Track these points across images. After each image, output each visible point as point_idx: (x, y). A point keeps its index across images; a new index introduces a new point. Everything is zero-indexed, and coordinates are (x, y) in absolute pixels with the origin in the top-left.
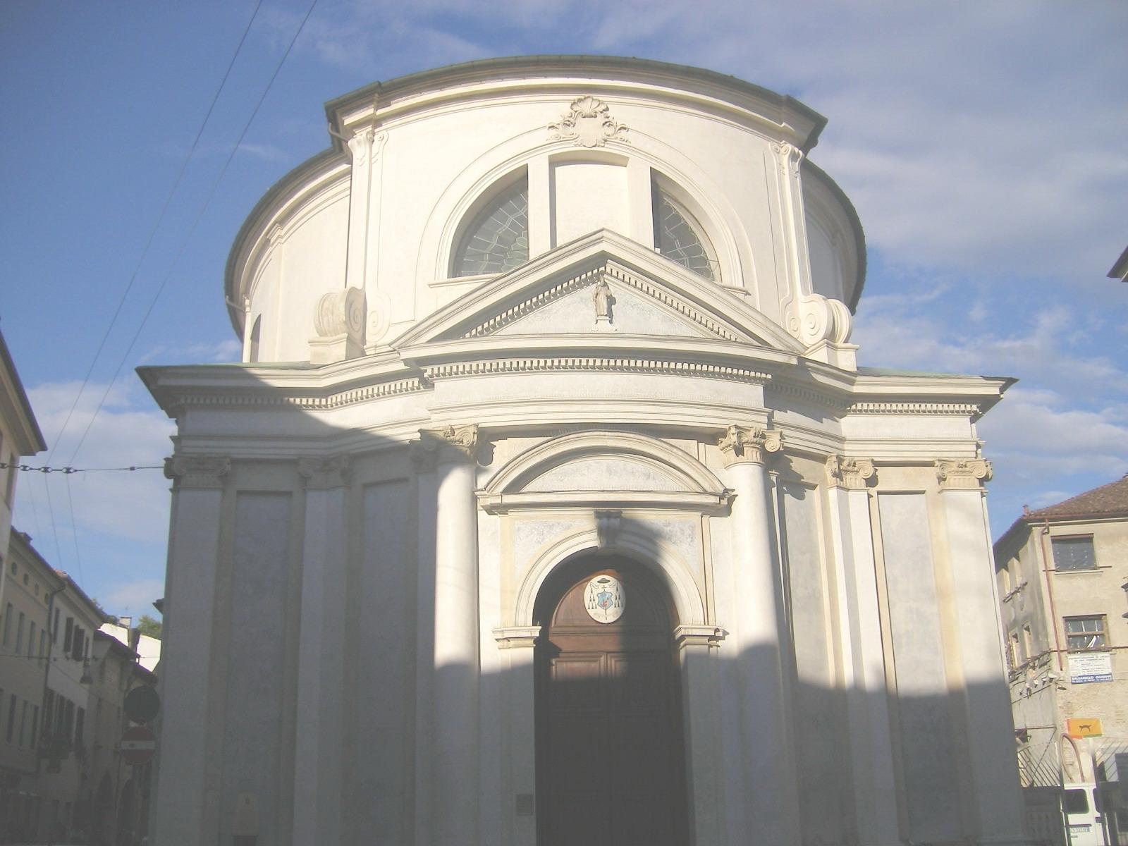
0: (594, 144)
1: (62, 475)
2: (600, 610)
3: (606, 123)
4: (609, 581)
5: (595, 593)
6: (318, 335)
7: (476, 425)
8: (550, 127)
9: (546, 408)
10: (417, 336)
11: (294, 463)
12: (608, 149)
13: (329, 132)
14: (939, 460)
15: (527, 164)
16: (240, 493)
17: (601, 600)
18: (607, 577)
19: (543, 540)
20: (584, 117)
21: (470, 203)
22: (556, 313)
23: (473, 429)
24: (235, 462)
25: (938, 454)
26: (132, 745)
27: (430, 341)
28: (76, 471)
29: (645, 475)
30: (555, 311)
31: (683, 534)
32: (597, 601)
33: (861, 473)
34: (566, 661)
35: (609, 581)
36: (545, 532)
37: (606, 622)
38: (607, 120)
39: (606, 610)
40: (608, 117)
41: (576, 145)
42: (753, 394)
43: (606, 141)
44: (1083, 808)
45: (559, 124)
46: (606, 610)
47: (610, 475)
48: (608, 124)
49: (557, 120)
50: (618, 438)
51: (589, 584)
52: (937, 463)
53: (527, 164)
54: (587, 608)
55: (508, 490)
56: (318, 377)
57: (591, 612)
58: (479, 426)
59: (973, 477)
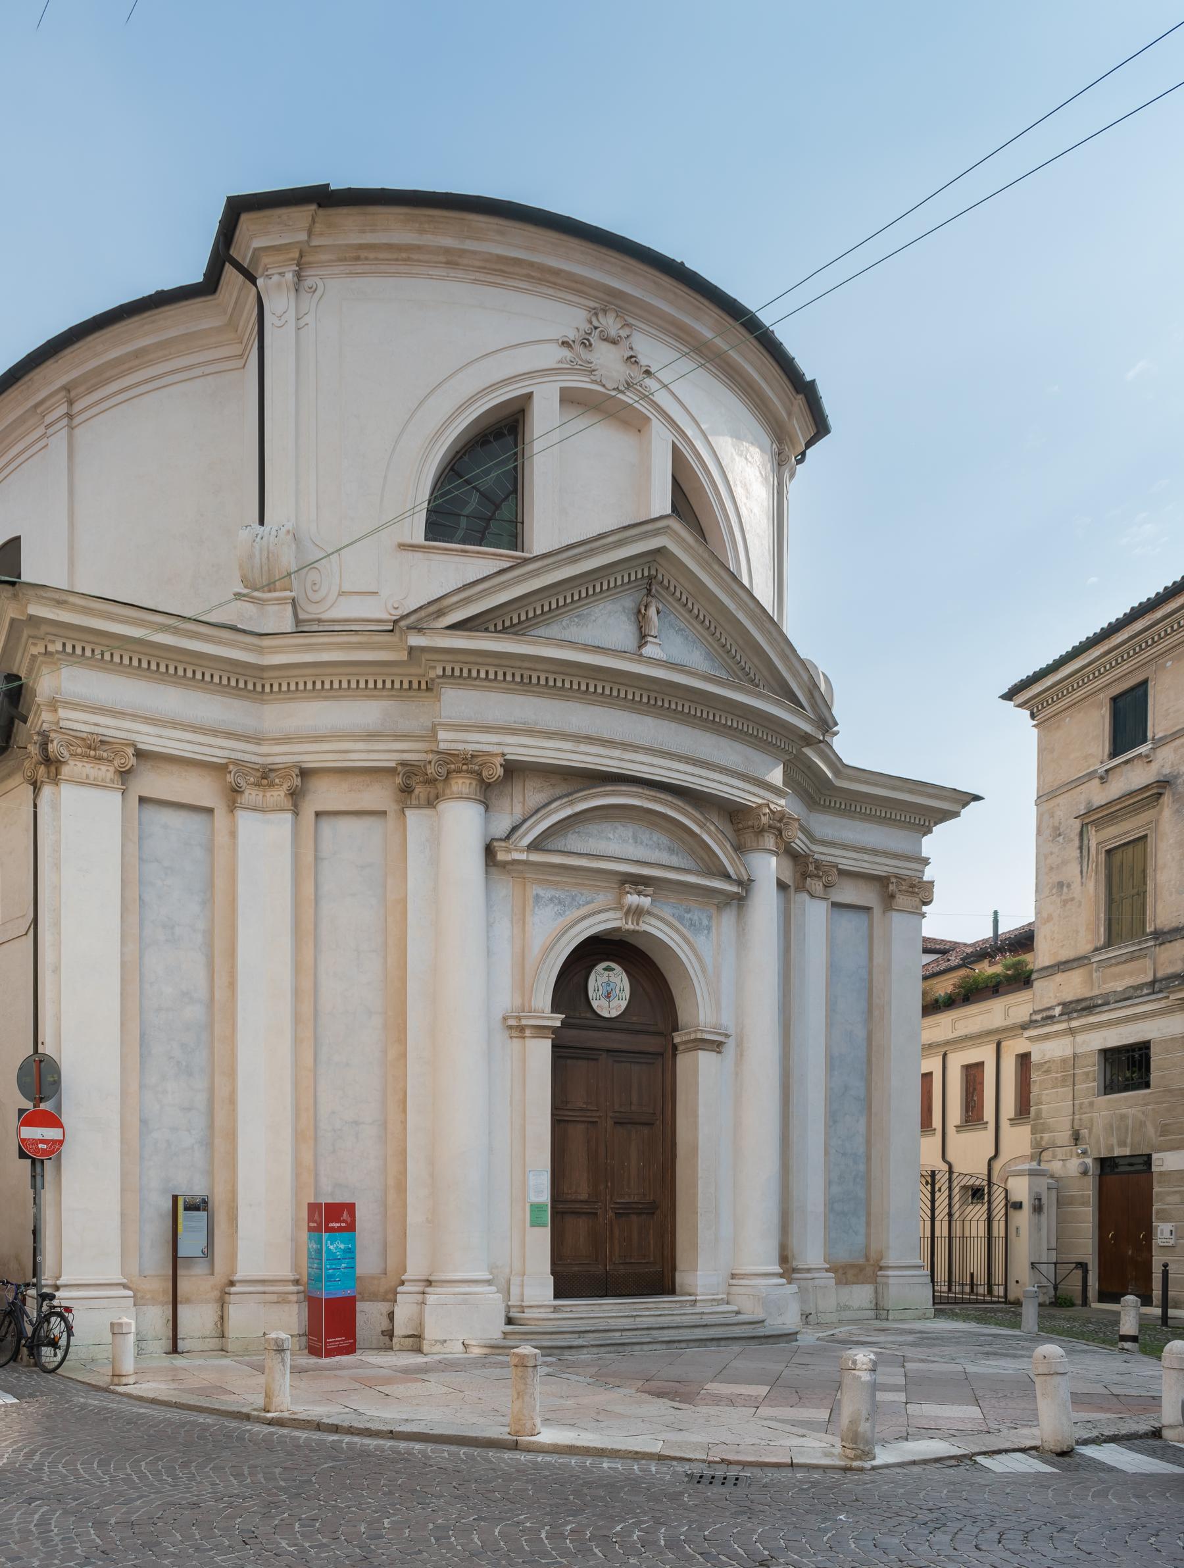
2: (604, 1002)
5: (599, 982)
7: (504, 755)
8: (563, 343)
9: (583, 748)
10: (440, 613)
11: (220, 769)
12: (628, 398)
14: (896, 877)
15: (532, 393)
16: (142, 800)
17: (605, 990)
18: (613, 965)
20: (605, 340)
22: (595, 621)
23: (500, 760)
24: (140, 754)
25: (896, 871)
30: (594, 618)
32: (601, 992)
34: (631, 1062)
37: (607, 1015)
44: (35, 1107)
45: (574, 342)
53: (532, 393)
54: (591, 998)
55: (534, 846)
56: (260, 650)
59: (918, 900)
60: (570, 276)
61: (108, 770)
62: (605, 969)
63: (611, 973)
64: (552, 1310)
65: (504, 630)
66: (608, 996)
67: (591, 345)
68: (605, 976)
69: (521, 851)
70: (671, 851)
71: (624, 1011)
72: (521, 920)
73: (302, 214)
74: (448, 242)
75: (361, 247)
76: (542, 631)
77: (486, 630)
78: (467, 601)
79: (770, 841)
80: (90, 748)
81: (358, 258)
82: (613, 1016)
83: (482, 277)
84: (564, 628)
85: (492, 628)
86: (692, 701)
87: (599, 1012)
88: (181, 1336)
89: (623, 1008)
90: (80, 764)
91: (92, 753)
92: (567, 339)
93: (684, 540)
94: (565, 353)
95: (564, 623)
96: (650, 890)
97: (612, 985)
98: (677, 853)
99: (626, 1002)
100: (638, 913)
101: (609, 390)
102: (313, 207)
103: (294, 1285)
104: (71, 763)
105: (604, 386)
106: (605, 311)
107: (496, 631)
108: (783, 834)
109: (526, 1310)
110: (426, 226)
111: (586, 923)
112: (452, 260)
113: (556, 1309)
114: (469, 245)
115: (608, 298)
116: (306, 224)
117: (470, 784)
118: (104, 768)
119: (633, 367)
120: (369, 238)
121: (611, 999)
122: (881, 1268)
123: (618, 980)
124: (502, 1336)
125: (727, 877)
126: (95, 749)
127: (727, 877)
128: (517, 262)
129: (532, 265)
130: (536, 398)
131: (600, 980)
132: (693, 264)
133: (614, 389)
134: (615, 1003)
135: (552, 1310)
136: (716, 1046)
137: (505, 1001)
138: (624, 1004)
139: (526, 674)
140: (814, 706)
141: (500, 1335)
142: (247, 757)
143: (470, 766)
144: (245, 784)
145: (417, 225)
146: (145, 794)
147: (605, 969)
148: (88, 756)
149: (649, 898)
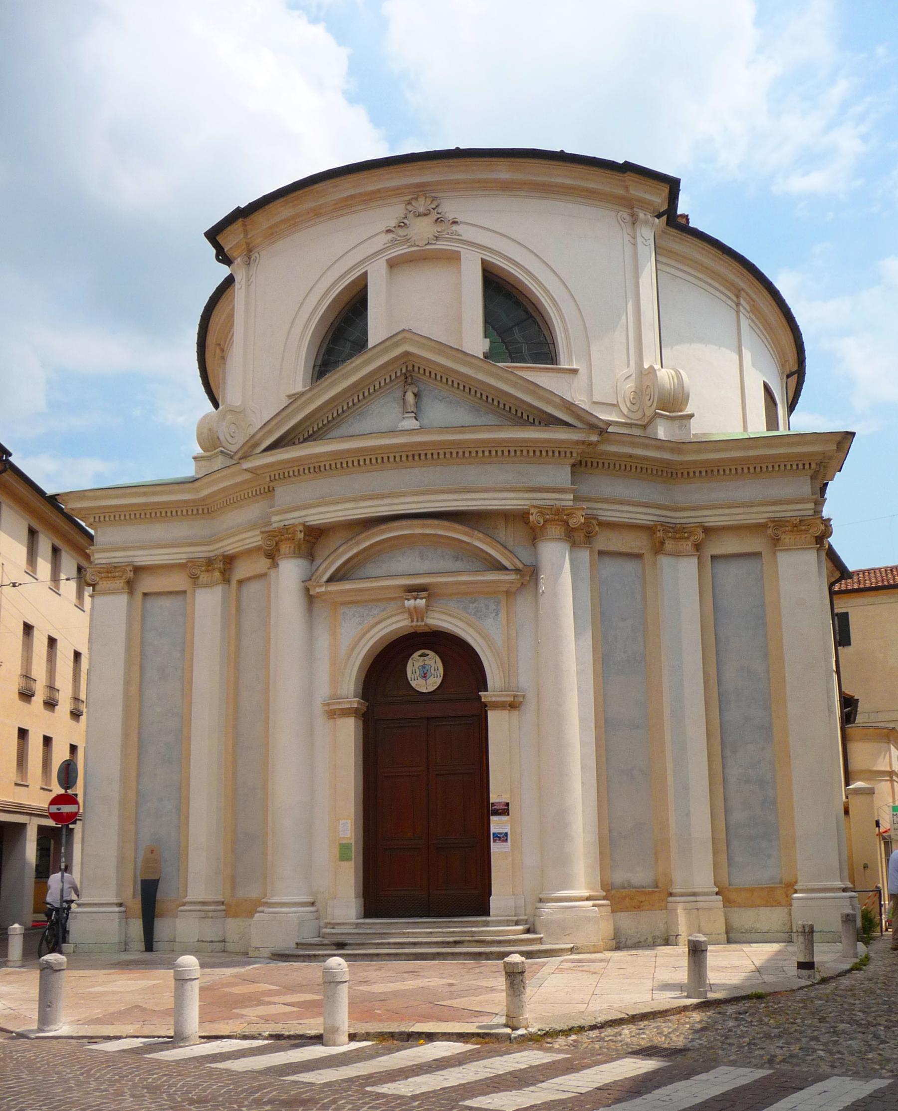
0: (427, 242)
1: (10, 589)
2: (421, 681)
3: (438, 219)
4: (428, 655)
6: (203, 452)
9: (362, 504)
10: (256, 445)
12: (441, 245)
13: (260, 256)
17: (422, 673)
19: (363, 621)
20: (419, 216)
21: (321, 313)
26: (59, 809)
27: (265, 450)
28: (20, 584)
29: (454, 557)
31: (488, 609)
32: (418, 673)
33: (692, 538)
35: (428, 655)
36: (365, 615)
37: (424, 691)
38: (439, 216)
39: (426, 680)
40: (440, 214)
41: (409, 246)
42: (561, 475)
43: (437, 237)
45: (395, 227)
46: (426, 680)
47: (422, 559)
48: (439, 220)
49: (392, 223)
50: (424, 526)
51: (411, 659)
52: (770, 524)
53: (367, 271)
54: (409, 679)
57: (413, 684)
58: (307, 524)
60: (387, 190)
61: (120, 583)
62: (420, 656)
63: (426, 658)
64: (354, 927)
65: (305, 440)
66: (425, 676)
67: (406, 224)
68: (420, 661)
69: (321, 586)
70: (456, 558)
71: (439, 686)
72: (333, 633)
73: (238, 225)
74: (311, 205)
75: (270, 228)
76: (336, 433)
77: (294, 444)
78: (270, 432)
79: (555, 530)
80: (108, 573)
81: (272, 234)
82: (430, 691)
83: (335, 214)
84: (350, 426)
85: (297, 442)
86: (260, 485)
87: (418, 689)
88: (157, 940)
89: (438, 684)
90: (105, 582)
91: (110, 575)
92: (389, 228)
93: (418, 342)
94: (390, 236)
95: (350, 423)
96: (424, 594)
97: (427, 667)
98: (462, 559)
99: (441, 678)
100: (414, 613)
101: (422, 247)
102: (240, 220)
103: (117, 907)
104: (100, 583)
105: (418, 246)
106: (416, 199)
107: (300, 443)
108: (570, 524)
109: (336, 927)
110: (296, 202)
111: (376, 629)
112: (317, 214)
113: (357, 925)
114: (322, 201)
115: (416, 190)
116: (241, 229)
117: (290, 547)
118: (118, 582)
119: (441, 224)
120: (272, 222)
121: (427, 677)
122: (671, 895)
123: (432, 663)
124: (296, 946)
125: (502, 568)
126: (111, 573)
127: (502, 568)
128: (352, 197)
129: (361, 194)
130: (368, 272)
131: (417, 665)
132: (465, 144)
133: (426, 245)
134: (431, 680)
135: (354, 927)
136: (513, 706)
137: (323, 691)
138: (439, 680)
139: (296, 469)
140: (578, 417)
141: (294, 946)
142: (197, 555)
143: (285, 536)
144: (199, 572)
145: (291, 204)
146: (145, 591)
147: (420, 656)
148: (109, 577)
149: (424, 600)
